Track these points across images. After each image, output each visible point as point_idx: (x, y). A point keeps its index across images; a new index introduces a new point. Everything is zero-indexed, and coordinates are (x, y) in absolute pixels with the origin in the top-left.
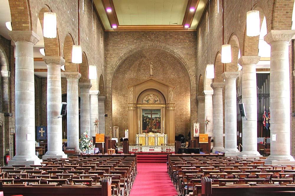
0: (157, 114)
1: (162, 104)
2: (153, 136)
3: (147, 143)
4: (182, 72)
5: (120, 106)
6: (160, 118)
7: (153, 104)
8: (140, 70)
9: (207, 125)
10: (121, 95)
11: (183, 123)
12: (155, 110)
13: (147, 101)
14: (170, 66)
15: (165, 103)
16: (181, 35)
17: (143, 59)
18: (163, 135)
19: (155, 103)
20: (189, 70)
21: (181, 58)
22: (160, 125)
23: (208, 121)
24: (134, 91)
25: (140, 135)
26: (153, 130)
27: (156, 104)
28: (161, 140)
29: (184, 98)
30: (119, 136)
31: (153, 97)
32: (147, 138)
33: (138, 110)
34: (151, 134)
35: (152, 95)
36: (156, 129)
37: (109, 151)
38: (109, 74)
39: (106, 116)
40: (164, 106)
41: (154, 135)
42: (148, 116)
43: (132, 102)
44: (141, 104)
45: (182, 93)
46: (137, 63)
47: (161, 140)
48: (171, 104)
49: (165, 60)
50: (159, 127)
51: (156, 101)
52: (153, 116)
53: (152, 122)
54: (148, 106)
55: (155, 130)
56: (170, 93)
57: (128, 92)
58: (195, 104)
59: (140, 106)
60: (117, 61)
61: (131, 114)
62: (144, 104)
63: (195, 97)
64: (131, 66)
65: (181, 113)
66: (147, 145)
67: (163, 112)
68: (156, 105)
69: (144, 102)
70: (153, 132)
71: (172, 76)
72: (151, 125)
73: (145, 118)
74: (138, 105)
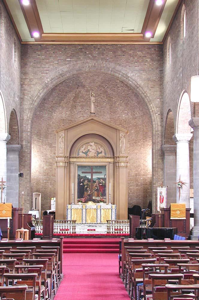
0: (101, 173)
1: (108, 158)
3: (84, 218)
4: (139, 109)
5: (44, 161)
6: (104, 179)
7: (94, 158)
9: (181, 189)
11: (139, 188)
12: (96, 167)
13: (86, 153)
14: (121, 101)
15: (112, 156)
16: (139, 51)
18: (109, 206)
19: (97, 155)
20: (150, 104)
21: (138, 86)
22: (104, 191)
23: (183, 183)
25: (74, 206)
26: (94, 198)
29: (142, 149)
30: (41, 207)
31: (94, 147)
32: (84, 210)
33: (72, 166)
34: (90, 204)
35: (93, 144)
36: (98, 196)
37: (19, 233)
38: (27, 111)
39: (21, 175)
40: (111, 160)
44: (75, 158)
45: (139, 142)
46: (71, 95)
48: (122, 157)
49: (114, 90)
50: (104, 194)
51: (99, 153)
52: (95, 177)
53: (92, 185)
54: (87, 160)
56: (120, 141)
58: (159, 157)
59: (75, 160)
60: (40, 91)
61: (61, 173)
63: (159, 147)
64: (62, 100)
65: (137, 173)
66: (84, 222)
68: (99, 160)
69: (81, 154)
70: (94, 201)
71: (124, 116)
72: (91, 191)
73: (82, 180)
74: (72, 160)
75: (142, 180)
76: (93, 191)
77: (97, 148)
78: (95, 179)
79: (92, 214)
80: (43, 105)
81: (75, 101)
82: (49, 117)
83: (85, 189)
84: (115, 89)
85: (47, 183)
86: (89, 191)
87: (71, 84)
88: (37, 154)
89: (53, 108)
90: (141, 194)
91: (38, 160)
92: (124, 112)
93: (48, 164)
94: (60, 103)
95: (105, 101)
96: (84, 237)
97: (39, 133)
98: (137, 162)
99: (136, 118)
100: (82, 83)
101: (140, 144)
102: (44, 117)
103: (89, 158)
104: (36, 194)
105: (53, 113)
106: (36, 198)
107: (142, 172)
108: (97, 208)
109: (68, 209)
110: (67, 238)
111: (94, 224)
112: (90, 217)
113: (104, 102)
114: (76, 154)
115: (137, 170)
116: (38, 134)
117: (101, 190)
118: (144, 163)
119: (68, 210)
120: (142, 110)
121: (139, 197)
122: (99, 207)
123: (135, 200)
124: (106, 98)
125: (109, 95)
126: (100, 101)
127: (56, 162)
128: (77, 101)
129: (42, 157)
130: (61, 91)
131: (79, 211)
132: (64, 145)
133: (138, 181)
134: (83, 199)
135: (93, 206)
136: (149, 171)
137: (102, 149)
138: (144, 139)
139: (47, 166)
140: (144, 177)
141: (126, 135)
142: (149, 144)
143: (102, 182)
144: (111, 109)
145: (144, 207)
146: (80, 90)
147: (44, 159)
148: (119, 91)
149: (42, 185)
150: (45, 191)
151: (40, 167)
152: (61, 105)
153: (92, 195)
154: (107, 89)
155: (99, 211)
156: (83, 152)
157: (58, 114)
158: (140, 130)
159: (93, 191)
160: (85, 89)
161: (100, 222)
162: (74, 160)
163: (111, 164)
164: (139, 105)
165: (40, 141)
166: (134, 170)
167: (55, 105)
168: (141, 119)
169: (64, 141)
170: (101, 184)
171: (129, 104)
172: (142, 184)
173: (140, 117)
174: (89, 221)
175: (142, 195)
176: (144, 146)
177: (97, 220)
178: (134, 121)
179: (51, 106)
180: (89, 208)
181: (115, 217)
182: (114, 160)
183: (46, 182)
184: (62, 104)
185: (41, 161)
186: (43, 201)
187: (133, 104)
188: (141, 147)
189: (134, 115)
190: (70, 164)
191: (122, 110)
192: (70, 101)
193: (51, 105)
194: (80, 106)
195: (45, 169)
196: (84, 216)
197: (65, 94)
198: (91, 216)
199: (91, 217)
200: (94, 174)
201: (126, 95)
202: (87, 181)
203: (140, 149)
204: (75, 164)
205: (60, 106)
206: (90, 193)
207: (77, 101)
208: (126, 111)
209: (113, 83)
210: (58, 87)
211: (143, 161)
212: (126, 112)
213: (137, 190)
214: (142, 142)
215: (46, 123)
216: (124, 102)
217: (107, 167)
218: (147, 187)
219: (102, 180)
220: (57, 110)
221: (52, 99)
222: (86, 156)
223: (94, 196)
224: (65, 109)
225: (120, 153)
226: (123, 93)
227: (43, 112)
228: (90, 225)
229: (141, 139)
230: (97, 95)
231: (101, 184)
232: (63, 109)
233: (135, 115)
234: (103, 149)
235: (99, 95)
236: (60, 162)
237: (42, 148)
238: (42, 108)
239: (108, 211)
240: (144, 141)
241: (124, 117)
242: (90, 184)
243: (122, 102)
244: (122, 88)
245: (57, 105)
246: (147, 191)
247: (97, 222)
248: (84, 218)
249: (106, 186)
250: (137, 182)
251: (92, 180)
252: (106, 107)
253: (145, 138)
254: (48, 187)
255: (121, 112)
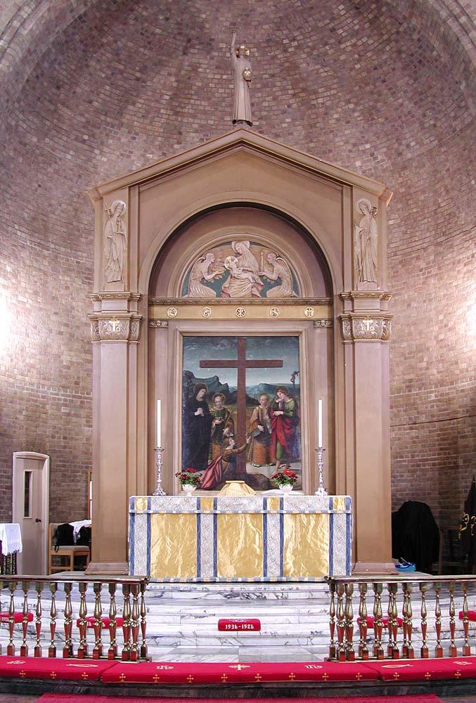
0: (278, 364)
1: (307, 303)
2: (252, 508)
3: (207, 557)
4: (422, 124)
5: (60, 333)
6: (293, 392)
7: (251, 304)
8: (180, 133)
10: (68, 270)
11: (423, 433)
12: (260, 340)
13: (216, 285)
14: (348, 102)
15: (323, 297)
17: (196, 56)
18: (321, 499)
19: (263, 293)
22: (293, 439)
24: (134, 217)
25: (161, 502)
26: (250, 468)
27: (273, 303)
28: (304, 537)
30: (51, 509)
31: (250, 261)
32: (207, 521)
33: (160, 340)
34: (235, 489)
35: (243, 247)
36: (267, 461)
40: (320, 313)
41: (261, 502)
42: (222, 382)
43: (119, 289)
44: (175, 303)
45: (418, 258)
46: (163, 81)
47: (304, 537)
48: (368, 296)
49: (321, 59)
50: (290, 453)
51: (267, 284)
52: (255, 380)
53: (243, 418)
54: (221, 312)
55: (267, 471)
56: (357, 230)
57: (97, 222)
59: (171, 312)
60: (20, 9)
61: (112, 363)
62: (196, 303)
64: (127, 98)
65: (412, 376)
66: (207, 574)
67: (316, 356)
68: (270, 312)
69: (198, 291)
70: (254, 482)
71: (358, 164)
72: (240, 439)
73: (201, 393)
74: (159, 312)
75: (434, 401)
76: (248, 441)
77: (260, 265)
78: (253, 389)
79: (245, 536)
80: (52, 108)
81: (178, 109)
82: (80, 167)
83: (213, 432)
84: (326, 54)
85: (76, 415)
86: (232, 442)
87: (158, 31)
88: (30, 301)
89: (97, 131)
90: (433, 456)
91: (35, 328)
92: (361, 148)
93: (76, 345)
94: (121, 113)
95: (290, 110)
96: (192, 693)
97: (41, 222)
98: (410, 334)
99: (405, 168)
100: (202, 28)
101: (423, 265)
102: (59, 163)
103: (230, 304)
104: (26, 458)
105: (97, 152)
106: (28, 474)
107: (435, 371)
108: (265, 508)
109: (133, 514)
110: (87, 693)
111: (252, 588)
112: (236, 552)
113: (284, 112)
114: (174, 289)
115: (411, 367)
116: (35, 224)
117: (281, 435)
118: (442, 337)
119: (133, 520)
120: (435, 126)
121: (423, 470)
122: (274, 506)
123: (405, 480)
124: (294, 95)
125: (304, 80)
126: (270, 109)
127: (95, 319)
128: (186, 110)
129: (54, 318)
130: (121, 57)
131: (184, 524)
132: (126, 249)
133: (416, 409)
134: (205, 475)
135: (245, 501)
136: (464, 366)
137: (280, 269)
138: (439, 244)
139: (72, 353)
140: (445, 389)
141: (380, 206)
142: (461, 257)
143: (284, 403)
144: (311, 142)
145: (442, 507)
146: (194, 60)
147: (60, 323)
148: (343, 57)
149: (55, 422)
150: (65, 447)
151: (45, 354)
152: (124, 121)
153: (244, 457)
154: (295, 54)
155: (273, 522)
156: (203, 281)
157: (114, 157)
158: (423, 210)
159: (248, 441)
160: (212, 58)
161: (278, 573)
162: (169, 313)
163: (318, 331)
164: (420, 107)
165: (46, 252)
166: (401, 368)
167: (103, 118)
168: (428, 165)
169: (126, 233)
170: (278, 413)
171: (379, 111)
172: (435, 419)
173: (425, 160)
174: (229, 571)
175: (432, 460)
176: (439, 268)
177: (265, 566)
178: (401, 180)
179: (88, 122)
180: (229, 511)
181: (348, 553)
182: (332, 312)
183: (68, 414)
184: (128, 117)
185: (51, 331)
186: (59, 485)
187: (396, 109)
188: (427, 278)
189: (400, 154)
190: (151, 329)
191: (353, 141)
192: (159, 109)
193: (87, 115)
194: (196, 131)
195: (64, 363)
196: (207, 544)
197: (138, 75)
198: (240, 547)
199: (240, 553)
200: (249, 372)
201: (368, 71)
202: (222, 400)
203: (424, 283)
204: (171, 330)
205: (122, 124)
206: (234, 448)
207: (186, 110)
208: (367, 142)
209: (320, 24)
210: (110, 38)
211: (436, 328)
212: (368, 146)
213: (414, 442)
214: (432, 258)
215: (71, 188)
216: (358, 108)
217: (303, 342)
218: (457, 428)
219: (281, 395)
220: (111, 141)
221: (87, 88)
222: (218, 295)
223: (251, 460)
224: (141, 139)
225: (356, 281)
226: (358, 66)
227: (56, 139)
228: (237, 588)
229: (425, 245)
230: (259, 86)
231: (278, 413)
232: (134, 138)
233: (404, 153)
234: (287, 264)
235: (265, 86)
236: (111, 318)
237: (51, 284)
238: (47, 123)
239: (316, 526)
240: (441, 249)
241: (361, 167)
242: (233, 410)
243: (351, 106)
244: (354, 41)
245: (109, 120)
246: (456, 443)
247: (265, 575)
248: (207, 557)
249: (299, 419)
250: (414, 414)
251: (240, 396)
252: (292, 134)
253: (444, 238)
254: (77, 434)
255: (350, 151)
